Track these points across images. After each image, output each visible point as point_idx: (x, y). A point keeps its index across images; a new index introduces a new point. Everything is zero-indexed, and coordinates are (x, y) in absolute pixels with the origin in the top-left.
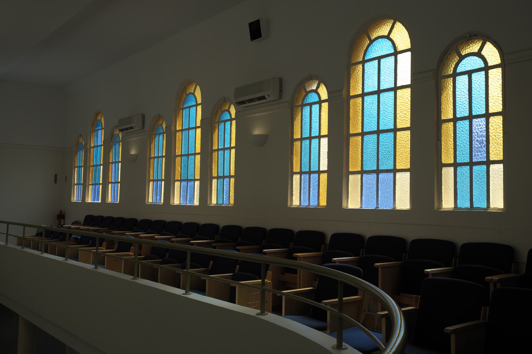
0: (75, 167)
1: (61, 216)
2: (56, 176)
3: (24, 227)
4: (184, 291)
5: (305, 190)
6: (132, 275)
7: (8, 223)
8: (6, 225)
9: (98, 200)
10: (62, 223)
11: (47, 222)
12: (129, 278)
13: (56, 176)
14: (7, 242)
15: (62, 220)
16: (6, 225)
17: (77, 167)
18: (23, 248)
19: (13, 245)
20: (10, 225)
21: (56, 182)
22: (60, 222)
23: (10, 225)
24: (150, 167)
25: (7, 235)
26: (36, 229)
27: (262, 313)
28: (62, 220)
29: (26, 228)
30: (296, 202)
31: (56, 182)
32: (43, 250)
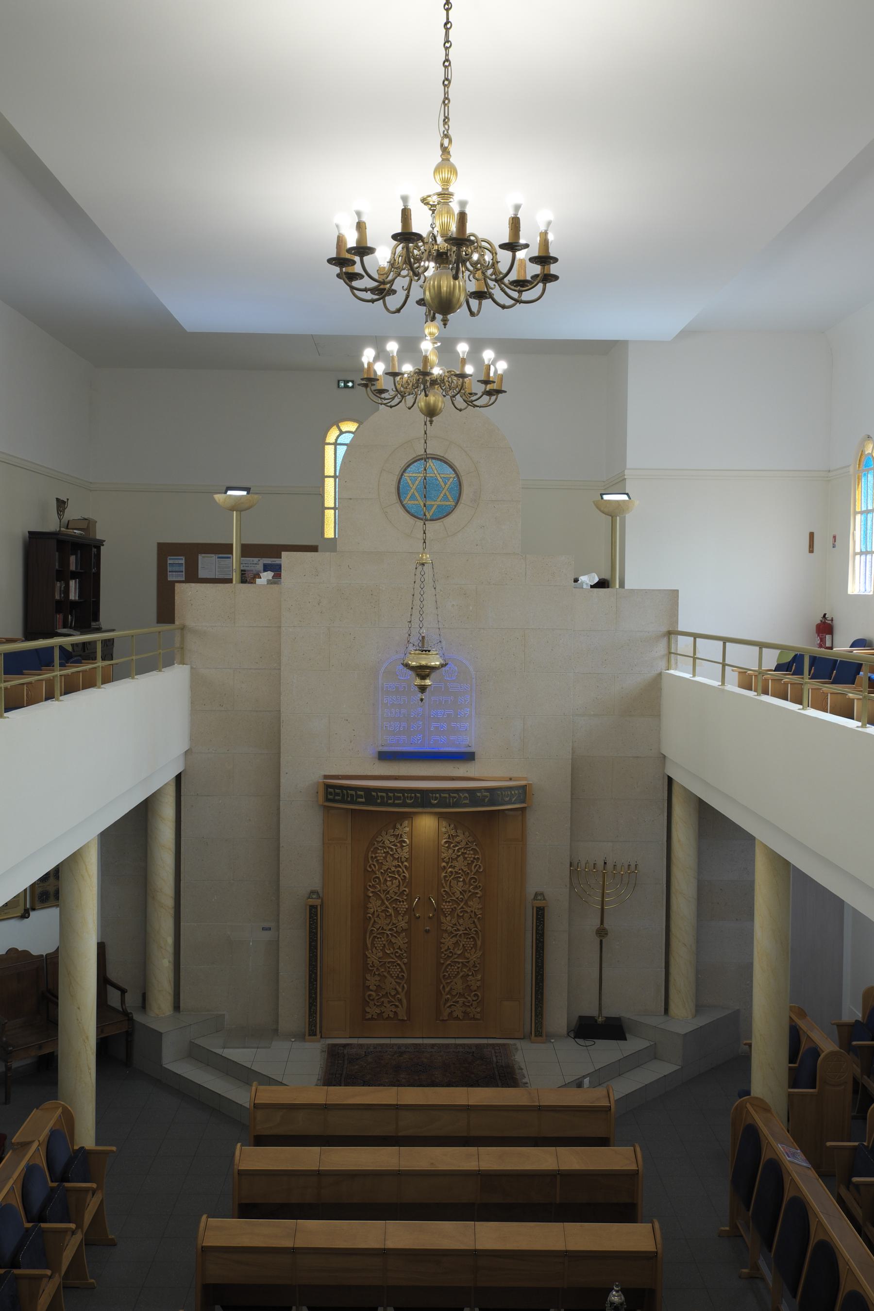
0: (856, 513)
1: (825, 628)
2: (812, 535)
3: (695, 639)
4: (860, 724)
5: (862, 577)
6: (801, 704)
7: (725, 640)
8: (721, 643)
9: (180, 562)
10: (828, 644)
11: (802, 640)
12: (795, 707)
13: (812, 535)
14: (723, 683)
15: (828, 637)
16: (721, 643)
17: (861, 513)
18: (863, 726)
19: (732, 687)
20: (728, 644)
21: (811, 550)
22: (823, 640)
23: (728, 644)
24: (855, 529)
25: (724, 665)
26: (777, 652)
27: (694, 675)
28: (828, 637)
29: (729, 645)
30: (169, 562)
31: (811, 550)
32: (760, 688)
